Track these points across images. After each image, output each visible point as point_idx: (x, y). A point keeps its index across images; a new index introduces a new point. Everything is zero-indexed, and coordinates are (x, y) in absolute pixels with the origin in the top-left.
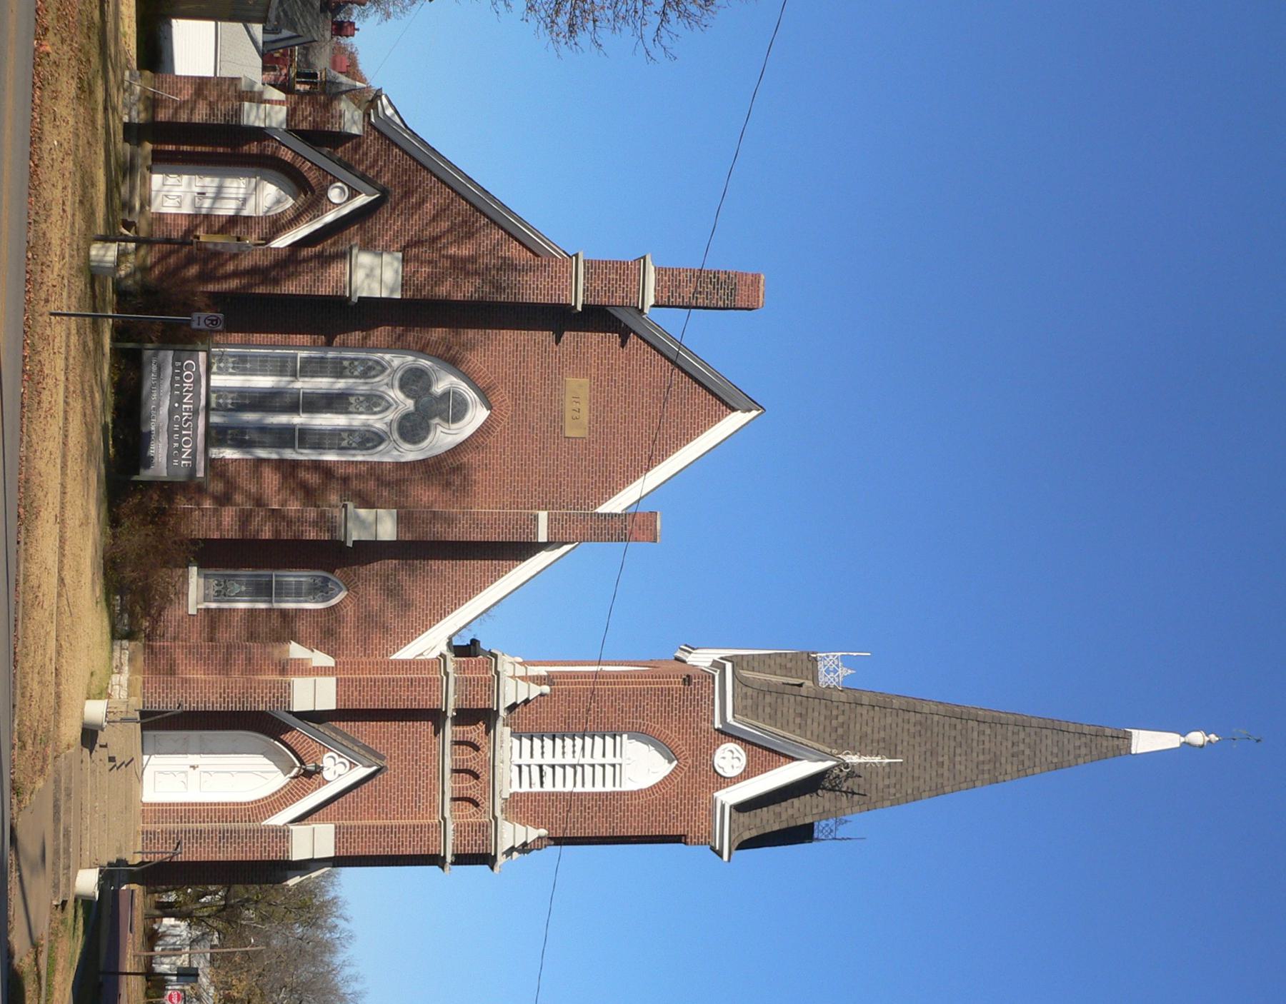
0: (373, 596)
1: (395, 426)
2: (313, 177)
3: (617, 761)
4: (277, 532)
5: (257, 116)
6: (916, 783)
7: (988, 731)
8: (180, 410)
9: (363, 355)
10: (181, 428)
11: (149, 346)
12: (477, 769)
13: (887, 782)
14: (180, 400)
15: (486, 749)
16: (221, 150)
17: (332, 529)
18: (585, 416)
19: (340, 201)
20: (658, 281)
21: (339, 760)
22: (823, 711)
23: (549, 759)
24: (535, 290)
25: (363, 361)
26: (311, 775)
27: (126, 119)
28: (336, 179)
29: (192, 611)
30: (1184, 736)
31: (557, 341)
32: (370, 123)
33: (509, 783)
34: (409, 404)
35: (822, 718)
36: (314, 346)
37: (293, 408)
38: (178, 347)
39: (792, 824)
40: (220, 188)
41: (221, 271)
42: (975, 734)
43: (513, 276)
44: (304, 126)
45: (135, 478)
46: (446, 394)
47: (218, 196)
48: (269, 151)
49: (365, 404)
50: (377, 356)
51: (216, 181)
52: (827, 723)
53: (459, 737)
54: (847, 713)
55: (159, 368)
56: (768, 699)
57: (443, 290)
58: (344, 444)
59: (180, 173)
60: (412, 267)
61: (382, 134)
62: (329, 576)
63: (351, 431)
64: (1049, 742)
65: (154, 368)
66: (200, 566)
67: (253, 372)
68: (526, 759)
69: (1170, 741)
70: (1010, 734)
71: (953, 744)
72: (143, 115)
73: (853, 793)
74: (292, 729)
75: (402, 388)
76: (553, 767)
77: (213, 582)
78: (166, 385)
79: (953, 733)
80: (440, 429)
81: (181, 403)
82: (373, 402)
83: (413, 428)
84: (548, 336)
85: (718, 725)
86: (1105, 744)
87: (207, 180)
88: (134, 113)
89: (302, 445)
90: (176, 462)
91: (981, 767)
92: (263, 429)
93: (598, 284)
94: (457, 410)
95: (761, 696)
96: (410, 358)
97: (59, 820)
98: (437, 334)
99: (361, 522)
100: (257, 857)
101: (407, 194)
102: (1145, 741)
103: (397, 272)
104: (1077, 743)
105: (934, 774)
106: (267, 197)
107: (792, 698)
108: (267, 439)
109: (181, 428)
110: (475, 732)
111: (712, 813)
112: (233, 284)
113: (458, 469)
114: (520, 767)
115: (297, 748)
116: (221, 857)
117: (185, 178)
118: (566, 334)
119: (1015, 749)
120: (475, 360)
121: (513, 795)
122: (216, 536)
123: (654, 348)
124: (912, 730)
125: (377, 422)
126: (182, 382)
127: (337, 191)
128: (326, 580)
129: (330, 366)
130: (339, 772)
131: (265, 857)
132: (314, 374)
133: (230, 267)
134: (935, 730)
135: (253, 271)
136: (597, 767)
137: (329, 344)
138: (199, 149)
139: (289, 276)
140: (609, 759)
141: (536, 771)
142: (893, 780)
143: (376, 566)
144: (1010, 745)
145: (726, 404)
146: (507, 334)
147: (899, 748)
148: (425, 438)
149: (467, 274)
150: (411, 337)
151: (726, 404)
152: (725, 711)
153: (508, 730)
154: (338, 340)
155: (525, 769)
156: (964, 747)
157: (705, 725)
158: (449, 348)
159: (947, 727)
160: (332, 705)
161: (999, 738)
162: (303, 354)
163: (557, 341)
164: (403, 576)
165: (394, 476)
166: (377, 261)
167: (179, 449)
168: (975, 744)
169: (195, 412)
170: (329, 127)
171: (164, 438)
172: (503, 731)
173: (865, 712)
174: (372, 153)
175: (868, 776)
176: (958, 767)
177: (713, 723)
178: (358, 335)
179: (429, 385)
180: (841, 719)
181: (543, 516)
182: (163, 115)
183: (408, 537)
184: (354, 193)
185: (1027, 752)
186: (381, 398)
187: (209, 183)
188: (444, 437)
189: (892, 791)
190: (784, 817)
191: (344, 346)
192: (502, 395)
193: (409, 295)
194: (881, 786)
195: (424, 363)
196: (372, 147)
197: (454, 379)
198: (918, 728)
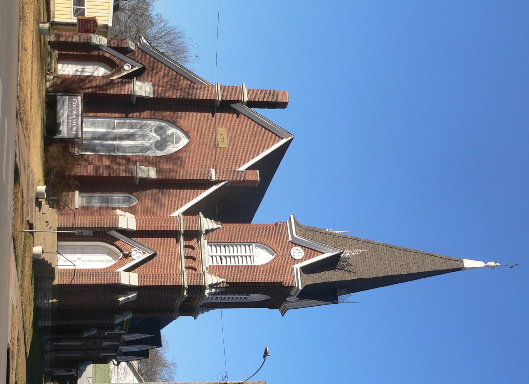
0: (148, 203)
1: (153, 145)
2: (118, 62)
3: (251, 254)
4: (110, 173)
5: (97, 40)
6: (376, 271)
7: (402, 253)
8: (71, 115)
9: (139, 121)
10: (72, 121)
11: (59, 94)
12: (195, 256)
13: (364, 268)
14: (72, 112)
15: (198, 248)
16: (83, 53)
17: (131, 172)
18: (226, 141)
19: (127, 68)
20: (248, 94)
21: (138, 251)
22: (333, 239)
23: (223, 254)
24: (202, 95)
25: (139, 123)
26: (127, 256)
27: (49, 40)
28: (126, 62)
29: (77, 207)
30: (486, 263)
31: (213, 116)
32: (138, 47)
33: (208, 262)
34: (159, 138)
35: (333, 242)
36: (121, 118)
37: (114, 139)
38: (71, 94)
39: (327, 281)
40: (83, 69)
41: (85, 86)
42: (397, 254)
43: (194, 91)
44: (114, 45)
45: (55, 137)
46: (172, 135)
47: (83, 71)
48: (101, 54)
49: (142, 138)
50: (145, 122)
51: (82, 67)
52: (335, 244)
53: (188, 255)
54: (343, 241)
55: (63, 102)
56: (310, 233)
57: (169, 95)
58: (134, 151)
59: (68, 64)
60: (156, 87)
61: (142, 51)
62: (130, 195)
63: (136, 147)
64: (429, 260)
65: (61, 102)
66: (80, 191)
67: (98, 127)
68: (214, 254)
69: (480, 264)
70: (412, 255)
71: (388, 257)
72: (55, 39)
73: (350, 272)
74: (119, 240)
75: (155, 132)
76: (226, 257)
77: (85, 199)
78: (66, 107)
79: (388, 253)
80: (171, 146)
81: (72, 113)
82: (144, 136)
83: (161, 145)
84: (209, 115)
85: (290, 239)
86: (452, 262)
87: (79, 66)
88: (51, 38)
89: (118, 151)
90: (70, 132)
91: (402, 267)
92: (102, 146)
93: (226, 93)
94: (178, 140)
95: (307, 232)
96: (157, 123)
97: (29, 189)
98: (167, 113)
99: (143, 171)
100: (106, 282)
101: (153, 69)
102: (468, 263)
103: (151, 88)
104: (441, 261)
105: (383, 267)
106: (101, 71)
107: (319, 234)
108: (105, 149)
109: (72, 121)
110: (193, 243)
111: (292, 273)
112: (90, 91)
113: (179, 158)
114: (212, 257)
115: (121, 247)
116: (91, 282)
117: (70, 65)
118: (216, 114)
119: (415, 261)
120: (182, 122)
121: (210, 266)
122: (86, 174)
123: (250, 118)
124: (371, 250)
125: (146, 143)
126: (72, 106)
127: (127, 67)
128: (130, 198)
129: (127, 125)
130: (137, 256)
131: (109, 282)
132: (121, 128)
133: (88, 85)
134: (380, 250)
135: (97, 87)
136: (244, 257)
137: (127, 117)
138: (75, 53)
139: (110, 88)
140: (248, 254)
141: (219, 258)
142: (366, 268)
143: (149, 191)
144: (412, 259)
145: (280, 137)
146: (194, 114)
147: (366, 256)
148: (165, 149)
149: (177, 90)
150: (157, 114)
151: (280, 137)
152: (293, 233)
153: (206, 242)
154: (130, 115)
155: (214, 258)
156: (394, 258)
157: (285, 240)
158: (172, 118)
159: (385, 250)
160: (136, 284)
161: (408, 256)
162: (116, 121)
163: (213, 116)
164: (160, 195)
165: (155, 161)
166: (143, 84)
167: (72, 128)
168: (398, 258)
169: (77, 116)
170: (123, 46)
171: (65, 124)
172: (204, 242)
173: (350, 241)
174: (139, 57)
175: (355, 266)
176: (392, 266)
177: (288, 239)
178: (136, 114)
179: (165, 132)
180: (341, 243)
181: (213, 171)
182: (62, 39)
183: (161, 177)
184: (133, 67)
185: (420, 263)
186: (147, 135)
187: (79, 67)
188: (171, 149)
189: (367, 272)
190: (323, 278)
191: (132, 118)
192: (193, 134)
193: (156, 96)
194: (361, 270)
195: (163, 124)
196: (139, 55)
197: (174, 129)
198: (373, 249)
